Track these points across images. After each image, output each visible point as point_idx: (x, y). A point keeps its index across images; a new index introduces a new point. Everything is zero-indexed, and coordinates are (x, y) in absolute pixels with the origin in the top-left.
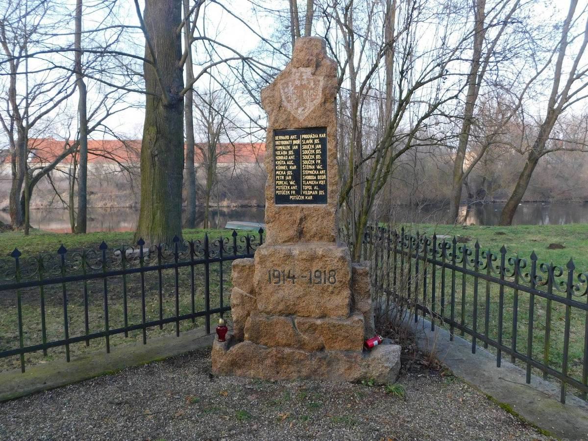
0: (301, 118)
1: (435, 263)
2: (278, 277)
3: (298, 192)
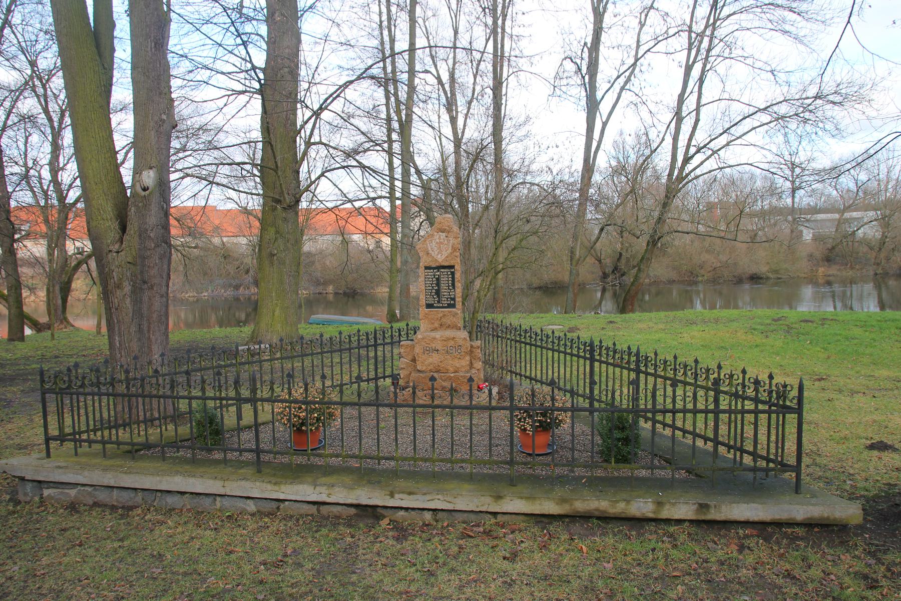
0: (440, 260)
1: (521, 342)
2: (428, 351)
3: (439, 302)
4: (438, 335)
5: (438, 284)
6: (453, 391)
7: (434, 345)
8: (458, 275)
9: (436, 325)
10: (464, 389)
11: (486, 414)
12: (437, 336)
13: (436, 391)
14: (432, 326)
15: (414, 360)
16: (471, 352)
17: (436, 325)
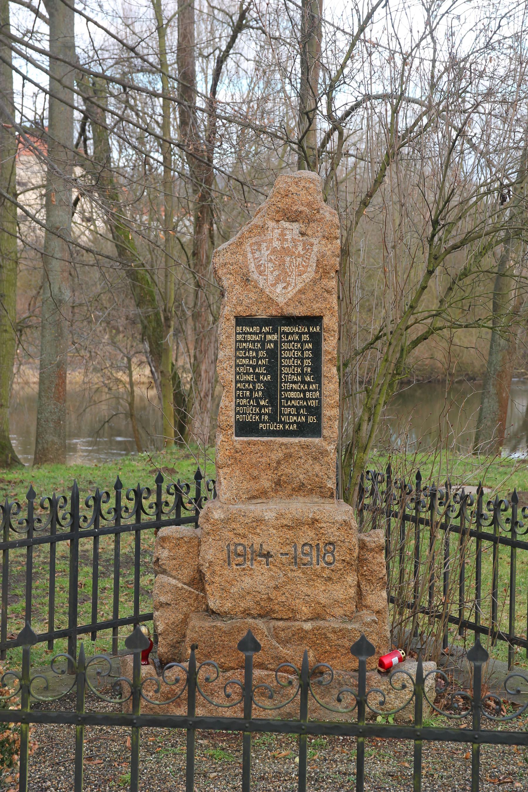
0: (281, 301)
3: (273, 418)
4: (268, 510)
5: (272, 368)
6: (308, 677)
7: (257, 540)
8: (330, 344)
9: (266, 483)
10: (342, 667)
11: (311, 717)
12: (269, 515)
13: (257, 673)
14: (254, 486)
15: (199, 581)
16: (361, 560)
17: (266, 483)
